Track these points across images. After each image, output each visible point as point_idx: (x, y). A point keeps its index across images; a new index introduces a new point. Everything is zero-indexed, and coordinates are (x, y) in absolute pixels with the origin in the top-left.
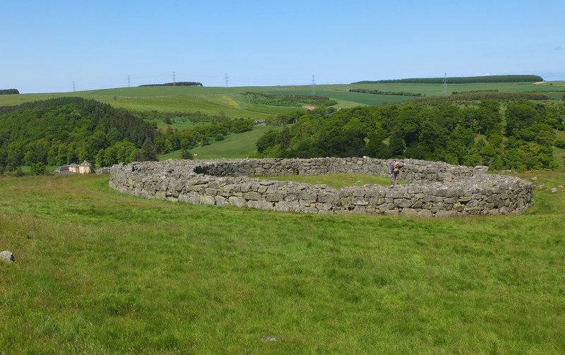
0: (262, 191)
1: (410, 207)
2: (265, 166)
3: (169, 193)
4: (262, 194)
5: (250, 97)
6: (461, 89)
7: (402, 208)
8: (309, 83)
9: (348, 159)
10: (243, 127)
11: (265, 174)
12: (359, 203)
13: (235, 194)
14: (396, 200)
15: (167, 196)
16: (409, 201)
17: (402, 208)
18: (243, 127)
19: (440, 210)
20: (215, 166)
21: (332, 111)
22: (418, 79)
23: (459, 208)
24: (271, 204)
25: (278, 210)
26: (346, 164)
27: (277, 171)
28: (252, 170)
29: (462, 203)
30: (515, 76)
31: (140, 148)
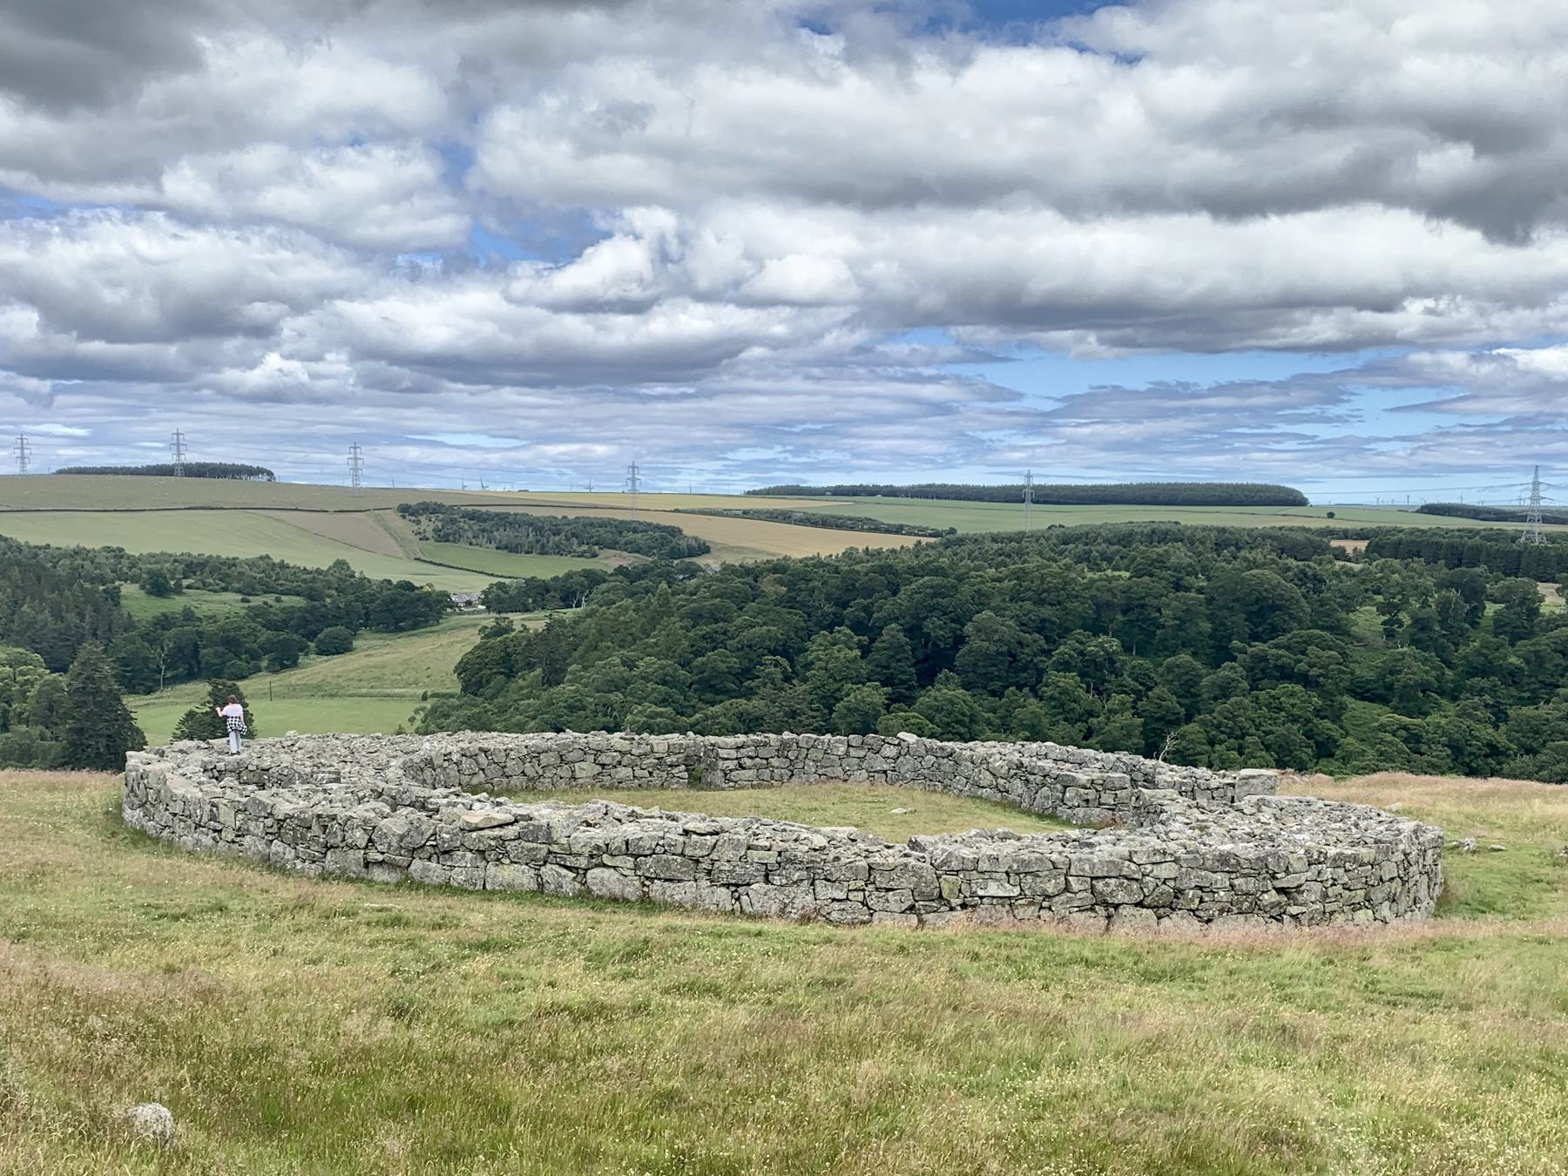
0: (698, 853)
1: (1140, 904)
2: (603, 759)
3: (374, 855)
4: (697, 862)
5: (428, 525)
6: (593, 514)
7: (1116, 907)
8: (1458, 502)
9: (855, 739)
10: (408, 611)
11: (606, 780)
12: (993, 889)
13: (606, 859)
14: (1100, 885)
15: (367, 865)
16: (1135, 886)
17: (1116, 907)
18: (408, 611)
19: (1221, 911)
20: (455, 757)
21: (692, 572)
22: (205, 465)
23: (1273, 905)
24: (723, 893)
25: (748, 909)
26: (847, 754)
27: (638, 772)
28: (564, 772)
29: (1280, 891)
30: (978, 487)
31: (63, 669)
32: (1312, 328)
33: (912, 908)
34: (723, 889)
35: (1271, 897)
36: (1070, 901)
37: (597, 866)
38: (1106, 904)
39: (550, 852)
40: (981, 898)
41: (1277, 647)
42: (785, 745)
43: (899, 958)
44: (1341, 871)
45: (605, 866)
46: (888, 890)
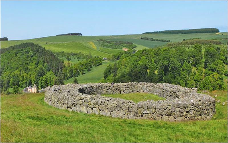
1: (166, 115)
7: (163, 115)
17: (163, 115)
18: (98, 62)
32: (127, 50)
33: (134, 116)
34: (109, 112)
35: (185, 113)
36: (156, 114)
37: (94, 107)
38: (161, 115)
39: (88, 105)
40: (144, 114)
41: (93, 80)
42: (131, 85)
43: (53, 90)
44: (196, 107)
45: (95, 107)
46: (131, 112)
